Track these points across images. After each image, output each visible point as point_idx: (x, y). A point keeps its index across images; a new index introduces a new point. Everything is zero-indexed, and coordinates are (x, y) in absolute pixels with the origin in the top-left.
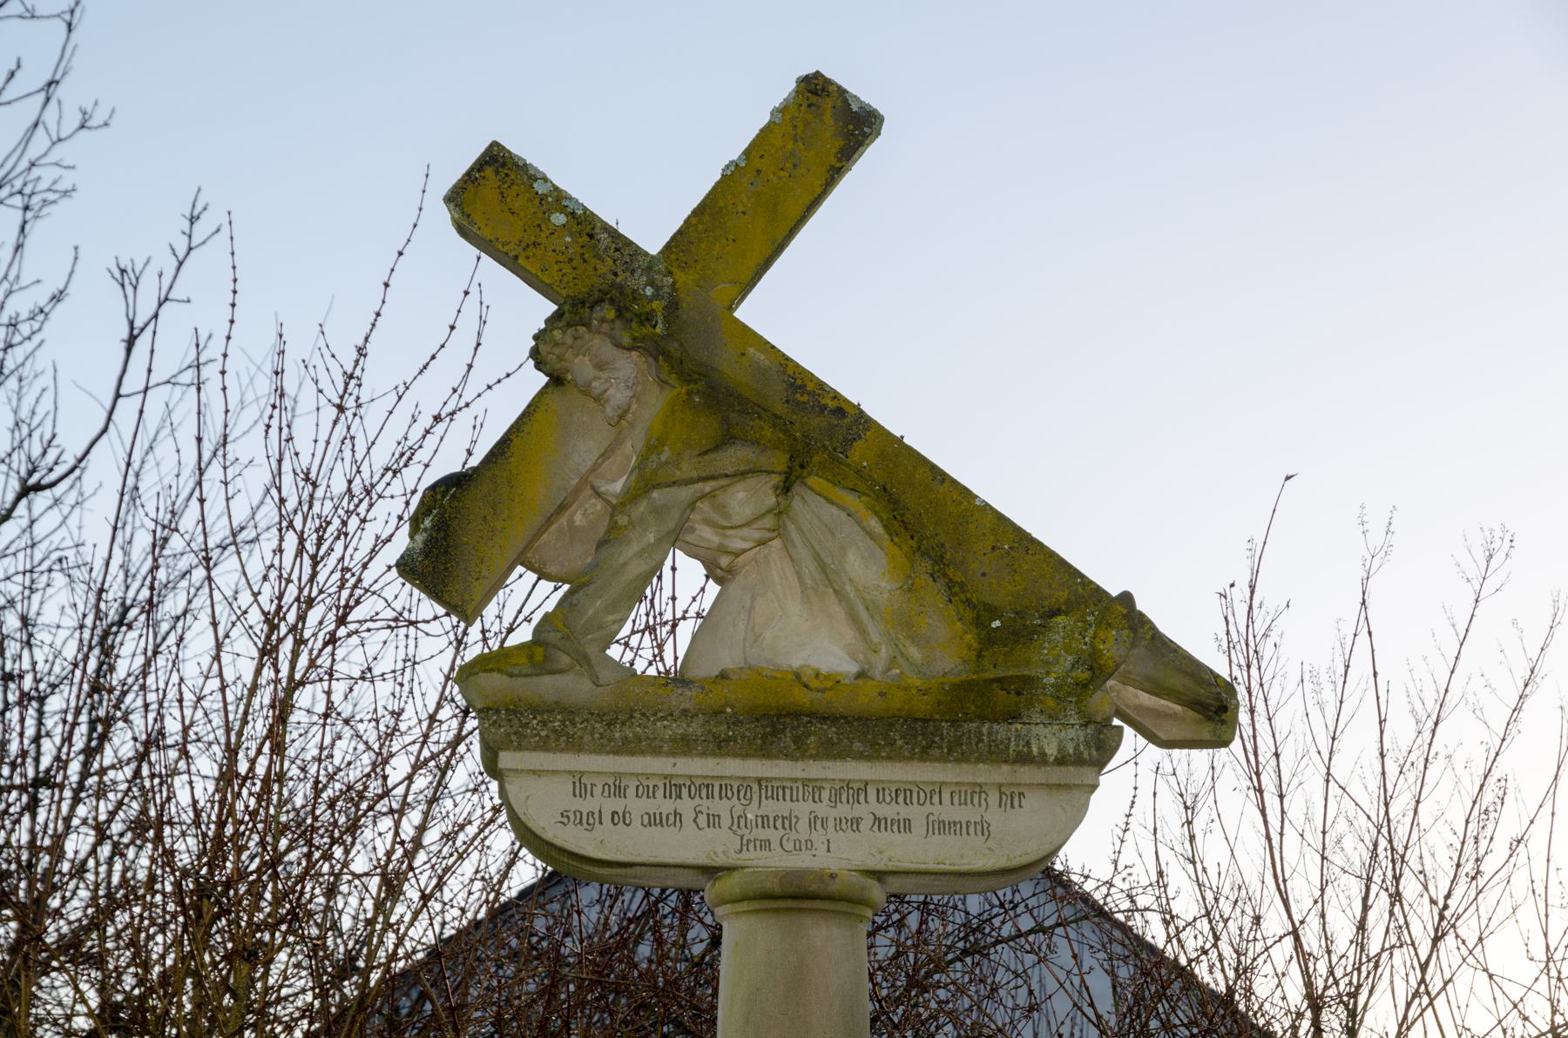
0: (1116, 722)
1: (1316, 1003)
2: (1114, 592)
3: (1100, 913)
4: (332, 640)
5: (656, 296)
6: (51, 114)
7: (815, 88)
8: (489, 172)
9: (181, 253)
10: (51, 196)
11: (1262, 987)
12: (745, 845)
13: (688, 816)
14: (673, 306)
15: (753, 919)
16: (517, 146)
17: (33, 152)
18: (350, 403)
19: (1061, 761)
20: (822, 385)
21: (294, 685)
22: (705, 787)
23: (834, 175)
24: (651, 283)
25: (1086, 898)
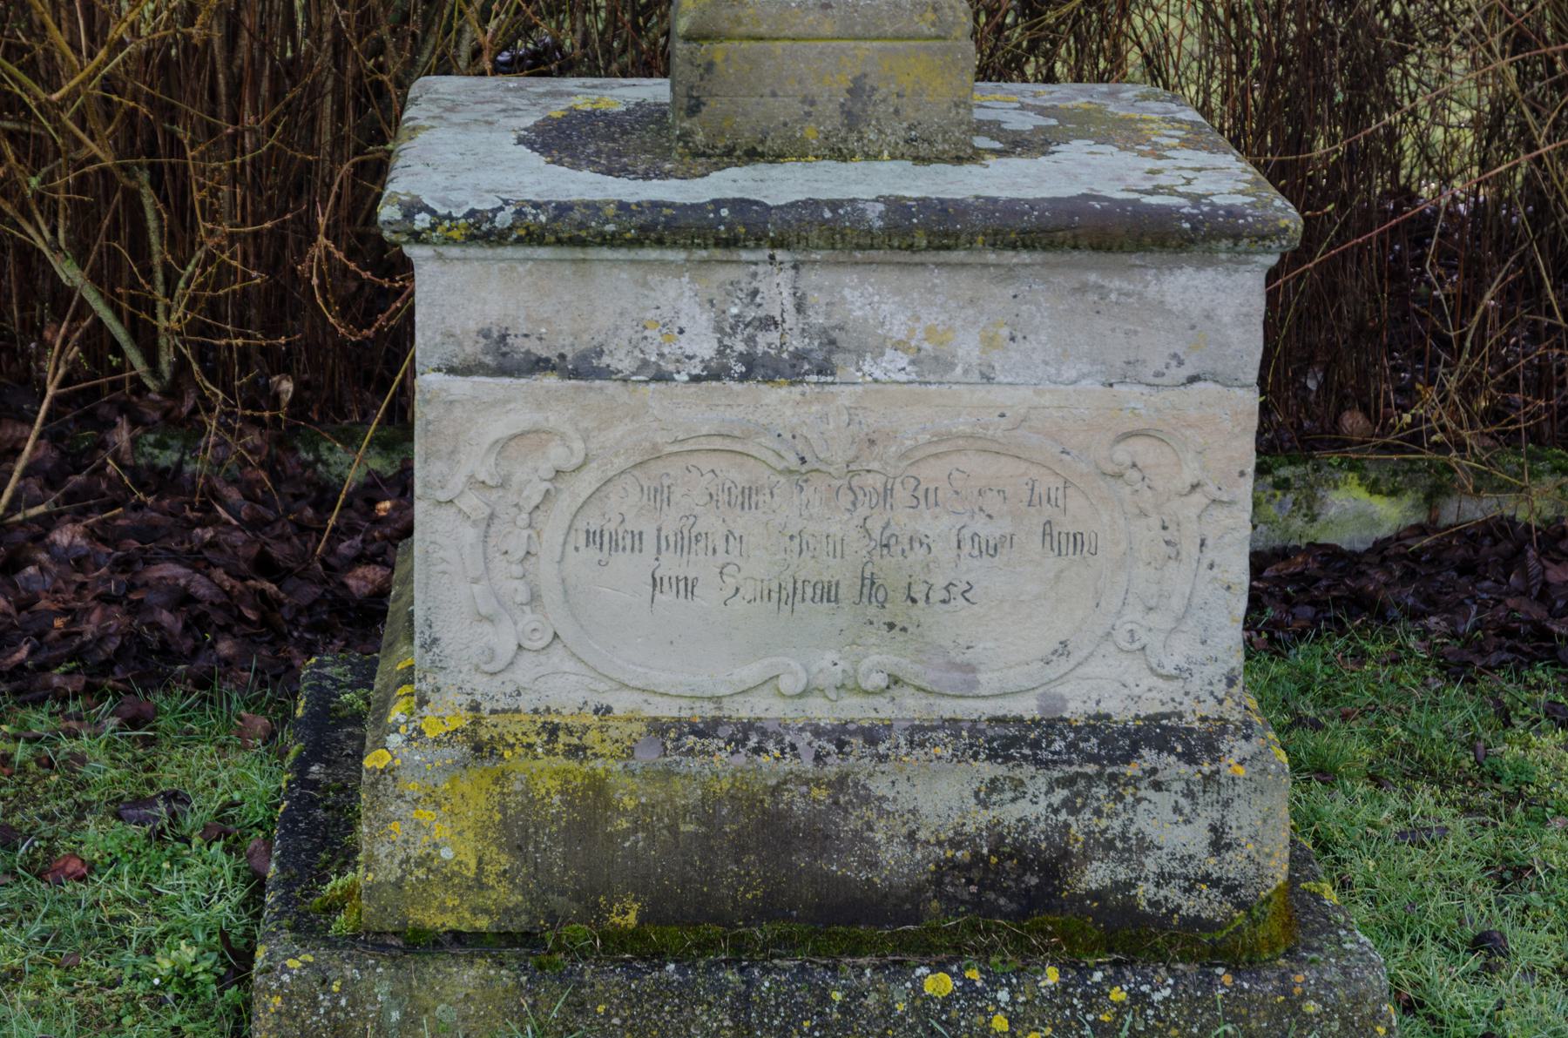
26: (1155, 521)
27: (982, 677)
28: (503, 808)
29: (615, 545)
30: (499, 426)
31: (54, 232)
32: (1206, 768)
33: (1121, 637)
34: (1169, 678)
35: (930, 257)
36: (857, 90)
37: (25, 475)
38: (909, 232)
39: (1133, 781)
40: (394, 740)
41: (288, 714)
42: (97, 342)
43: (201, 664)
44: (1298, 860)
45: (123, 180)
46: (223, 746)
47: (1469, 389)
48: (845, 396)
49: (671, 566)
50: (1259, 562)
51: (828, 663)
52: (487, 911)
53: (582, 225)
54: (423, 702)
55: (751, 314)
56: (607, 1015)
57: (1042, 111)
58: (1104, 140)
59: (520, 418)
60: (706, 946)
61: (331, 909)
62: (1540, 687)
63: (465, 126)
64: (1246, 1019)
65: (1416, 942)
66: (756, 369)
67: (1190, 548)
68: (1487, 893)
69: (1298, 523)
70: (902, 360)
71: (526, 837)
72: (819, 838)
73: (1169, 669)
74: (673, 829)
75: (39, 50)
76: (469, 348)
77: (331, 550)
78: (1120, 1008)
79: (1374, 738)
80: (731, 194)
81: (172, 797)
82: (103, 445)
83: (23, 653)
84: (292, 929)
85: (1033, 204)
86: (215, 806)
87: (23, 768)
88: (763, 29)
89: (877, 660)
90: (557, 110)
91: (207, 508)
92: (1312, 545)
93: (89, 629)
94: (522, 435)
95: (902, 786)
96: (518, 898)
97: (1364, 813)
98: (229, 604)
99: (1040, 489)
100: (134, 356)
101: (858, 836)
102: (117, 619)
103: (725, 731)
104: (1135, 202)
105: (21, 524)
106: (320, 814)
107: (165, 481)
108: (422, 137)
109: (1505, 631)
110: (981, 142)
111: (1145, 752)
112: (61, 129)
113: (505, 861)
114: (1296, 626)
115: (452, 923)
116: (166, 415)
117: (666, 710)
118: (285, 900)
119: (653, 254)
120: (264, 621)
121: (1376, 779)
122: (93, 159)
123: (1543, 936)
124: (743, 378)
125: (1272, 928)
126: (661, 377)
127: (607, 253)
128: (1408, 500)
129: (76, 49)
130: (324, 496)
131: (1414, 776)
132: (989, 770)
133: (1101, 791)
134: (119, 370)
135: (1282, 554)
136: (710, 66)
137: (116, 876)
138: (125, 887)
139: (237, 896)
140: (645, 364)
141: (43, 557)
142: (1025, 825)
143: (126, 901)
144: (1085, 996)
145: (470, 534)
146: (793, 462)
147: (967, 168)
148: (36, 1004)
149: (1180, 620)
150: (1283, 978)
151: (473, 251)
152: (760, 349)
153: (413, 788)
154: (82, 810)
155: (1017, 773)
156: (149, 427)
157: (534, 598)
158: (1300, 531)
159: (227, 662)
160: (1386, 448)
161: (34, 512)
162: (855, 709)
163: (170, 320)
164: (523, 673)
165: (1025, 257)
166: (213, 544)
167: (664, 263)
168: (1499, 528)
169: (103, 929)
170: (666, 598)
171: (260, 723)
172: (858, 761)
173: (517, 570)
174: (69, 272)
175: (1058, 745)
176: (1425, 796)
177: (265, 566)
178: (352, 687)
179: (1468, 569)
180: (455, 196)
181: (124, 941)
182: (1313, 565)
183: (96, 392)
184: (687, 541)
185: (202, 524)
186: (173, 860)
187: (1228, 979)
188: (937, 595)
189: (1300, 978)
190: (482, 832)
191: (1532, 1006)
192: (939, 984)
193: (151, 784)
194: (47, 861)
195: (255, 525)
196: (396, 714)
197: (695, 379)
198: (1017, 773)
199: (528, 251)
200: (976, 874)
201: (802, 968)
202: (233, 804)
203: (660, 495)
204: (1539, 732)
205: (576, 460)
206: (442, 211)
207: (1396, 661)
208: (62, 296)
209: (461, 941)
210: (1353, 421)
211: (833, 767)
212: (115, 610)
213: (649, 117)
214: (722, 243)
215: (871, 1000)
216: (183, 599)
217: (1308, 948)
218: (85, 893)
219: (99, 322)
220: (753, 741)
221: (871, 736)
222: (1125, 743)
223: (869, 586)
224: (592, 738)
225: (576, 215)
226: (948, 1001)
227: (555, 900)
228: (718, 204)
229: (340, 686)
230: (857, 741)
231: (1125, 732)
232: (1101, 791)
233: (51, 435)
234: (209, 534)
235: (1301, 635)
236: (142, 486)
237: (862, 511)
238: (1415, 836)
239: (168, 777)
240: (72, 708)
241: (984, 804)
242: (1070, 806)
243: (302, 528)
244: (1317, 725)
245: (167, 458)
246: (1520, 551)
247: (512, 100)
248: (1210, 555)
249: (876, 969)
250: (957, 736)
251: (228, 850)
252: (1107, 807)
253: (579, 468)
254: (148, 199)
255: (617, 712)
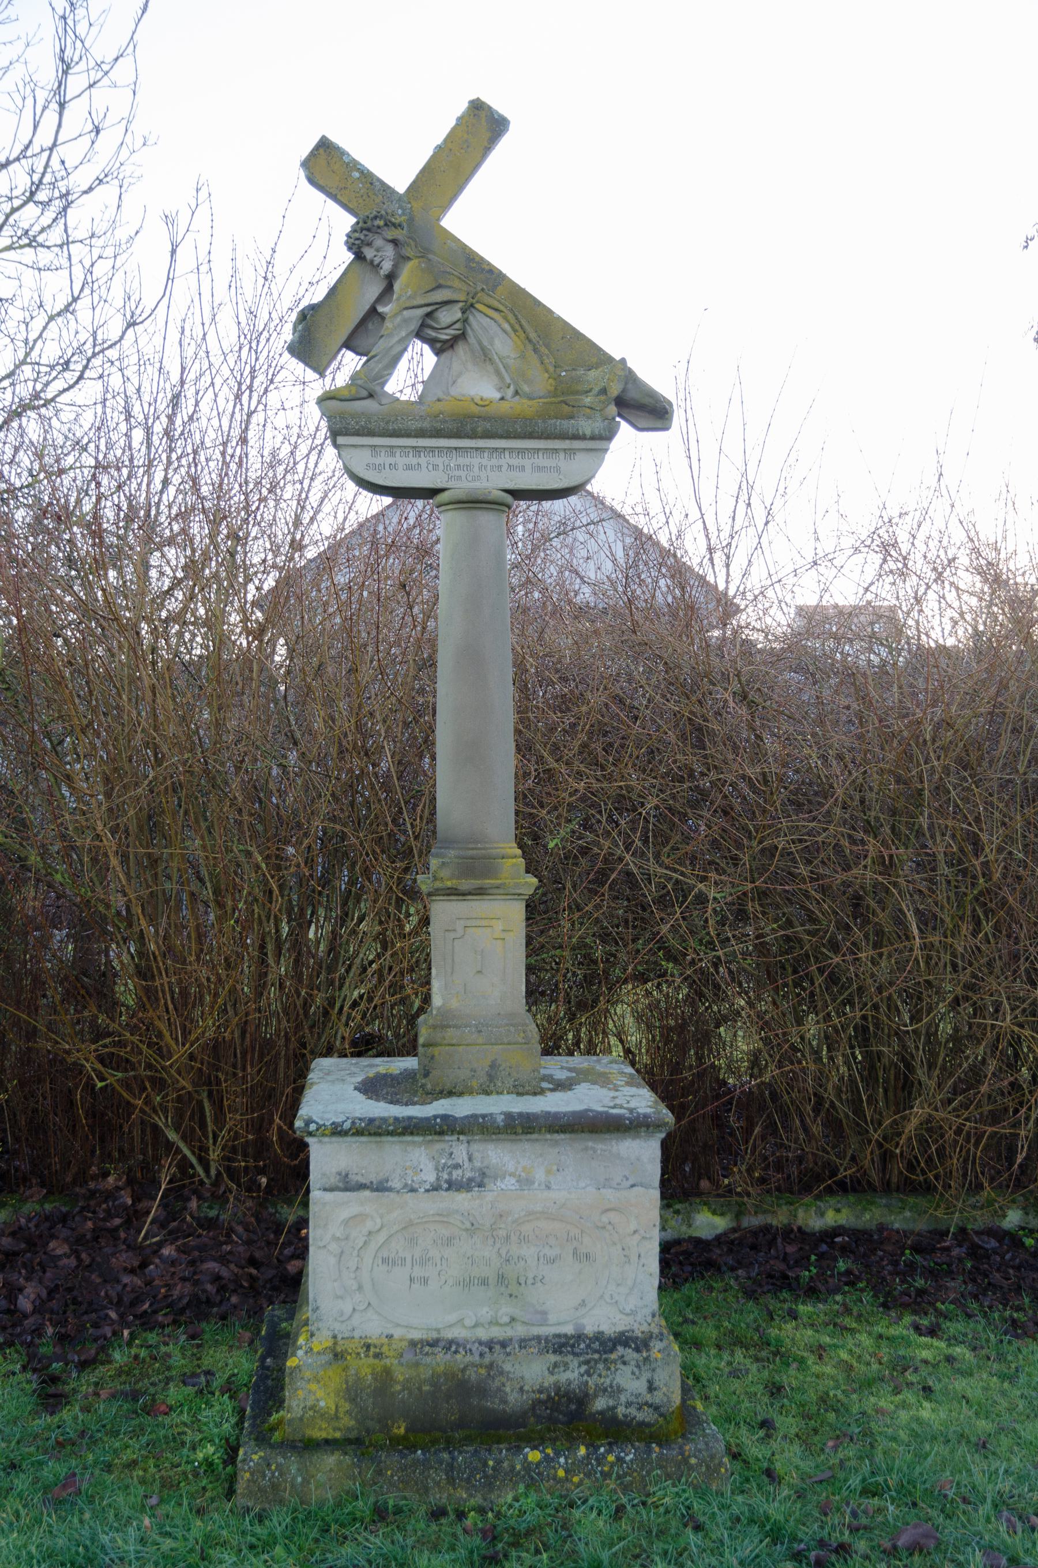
0: (618, 419)
1: (711, 550)
2: (618, 358)
3: (620, 516)
4: (266, 391)
5: (403, 214)
6: (129, 139)
7: (477, 107)
8: (321, 151)
9: (193, 207)
10: (132, 180)
11: (689, 544)
12: (450, 478)
13: (424, 465)
14: (411, 220)
15: (454, 513)
16: (334, 138)
17: (121, 159)
18: (269, 276)
19: (593, 438)
20: (482, 258)
21: (250, 415)
22: (432, 449)
23: (487, 150)
24: (400, 207)
25: (612, 509)
26: (619, 1247)
27: (550, 1317)
28: (347, 1382)
29: (394, 1263)
30: (345, 1214)
31: (166, 1118)
32: (645, 1354)
33: (607, 1297)
34: (627, 1315)
35: (523, 1137)
36: (493, 1065)
37: (152, 1223)
38: (514, 1127)
39: (614, 1362)
40: (300, 1353)
41: (259, 1332)
42: (184, 1165)
43: (223, 1308)
44: (685, 1390)
45: (195, 1096)
46: (231, 1347)
47: (750, 1170)
48: (489, 1196)
49: (418, 1272)
50: (665, 1248)
51: (485, 1312)
52: (339, 1429)
53: (379, 1127)
54: (312, 1335)
55: (450, 1162)
56: (392, 1476)
57: (570, 1070)
58: (594, 1083)
59: (354, 1209)
60: (434, 1442)
61: (273, 1429)
62: (784, 1301)
63: (333, 1082)
64: (666, 1467)
65: (737, 1424)
66: (453, 1186)
67: (634, 1258)
68: (766, 1399)
69: (684, 1228)
70: (513, 1181)
71: (356, 1396)
72: (482, 1391)
73: (628, 1311)
74: (420, 1389)
75: (162, 1044)
76: (332, 1180)
77: (281, 1253)
78: (612, 1465)
79: (717, 1328)
80: (442, 1112)
81: (208, 1373)
82: (185, 1208)
83: (146, 1306)
84: (256, 1439)
85: (565, 1114)
86: (226, 1376)
87: (144, 1360)
88: (454, 1041)
89: (506, 1311)
90: (371, 1073)
91: (228, 1236)
92: (690, 1238)
93: (176, 1293)
94: (355, 1216)
95: (517, 1366)
96: (353, 1423)
97: (714, 1363)
98: (236, 1280)
99: (572, 1234)
100: (200, 1170)
101: (499, 1389)
102: (188, 1288)
103: (442, 1344)
104: (606, 1113)
105: (149, 1245)
106: (270, 1382)
107: (210, 1224)
108: (315, 1087)
109: (770, 1276)
110: (545, 1085)
111: (619, 1348)
112: (171, 1077)
113: (347, 1406)
114: (684, 1276)
115: (324, 1435)
116: (212, 1195)
117: (416, 1335)
118: (253, 1426)
119: (409, 1138)
120: (251, 1287)
121: (719, 1347)
122: (184, 1088)
123: (790, 1419)
124: (447, 1190)
125: (675, 1425)
126: (413, 1190)
127: (390, 1138)
128: (728, 1217)
129: (177, 1042)
130: (278, 1228)
131: (735, 1345)
132: (553, 1358)
133: (601, 1366)
134: (194, 1176)
135: (678, 1242)
136: (433, 1057)
137: (182, 1412)
138: (185, 1417)
139: (233, 1420)
140: (406, 1185)
141: (157, 1261)
142: (569, 1382)
143: (185, 1424)
144: (597, 1459)
145: (332, 1260)
146: (468, 1225)
147: (539, 1098)
148: (144, 1477)
149: (632, 1289)
150: (681, 1448)
151: (334, 1139)
152: (454, 1177)
153: (307, 1374)
154: (168, 1380)
155: (565, 1359)
156: (205, 1200)
157: (360, 1288)
158: (685, 1232)
159: (235, 1307)
160: (718, 1196)
161: (155, 1240)
162: (497, 1333)
163: (214, 1155)
164: (356, 1321)
165: (562, 1136)
166: (230, 1252)
167: (414, 1142)
168: (766, 1229)
169: (174, 1438)
170: (416, 1286)
171: (247, 1335)
172: (498, 1355)
173: (352, 1275)
174: (172, 1136)
175: (582, 1346)
176: (739, 1354)
177: (253, 1262)
178: (286, 1320)
179: (754, 1247)
180: (327, 1116)
181: (183, 1444)
182: (691, 1247)
183: (184, 1186)
184: (424, 1261)
185: (226, 1243)
186: (206, 1404)
187: (657, 1449)
188: (529, 1282)
189: (687, 1448)
190: (337, 1393)
191: (786, 1454)
192: (534, 1456)
193: (199, 1366)
194: (152, 1406)
195: (249, 1243)
196: (301, 1341)
197: (427, 1191)
198: (565, 1359)
199: (357, 1138)
200: (549, 1405)
201: (476, 1451)
202: (234, 1375)
203: (413, 1241)
204: (785, 1322)
205: (378, 1227)
206: (321, 1122)
207: (726, 1291)
208: (169, 1145)
209: (329, 1444)
210: (704, 1184)
211: (487, 1360)
212: (188, 1284)
213: (409, 1076)
214: (436, 1133)
215: (505, 1464)
216: (217, 1278)
217: (691, 1433)
218: (167, 1420)
219: (185, 1157)
220: (453, 1348)
221: (504, 1344)
222: (610, 1344)
223: (501, 1278)
224: (385, 1349)
225: (377, 1123)
226: (538, 1464)
227: (370, 1424)
228: (435, 1117)
229: (282, 1320)
230: (497, 1347)
231: (610, 1339)
232: (601, 1366)
233: (164, 1205)
234: (229, 1248)
235: (686, 1280)
236: (201, 1226)
237: (498, 1245)
238: (735, 1374)
239: (207, 1363)
240: (167, 1331)
241: (552, 1373)
242: (588, 1373)
243: (269, 1243)
244: (693, 1323)
245: (212, 1213)
246: (775, 1239)
247: (354, 1069)
248: (643, 1260)
249: (508, 1450)
250: (540, 1343)
251: (231, 1398)
252: (604, 1373)
253: (379, 1230)
254: (207, 1104)
255: (396, 1336)
